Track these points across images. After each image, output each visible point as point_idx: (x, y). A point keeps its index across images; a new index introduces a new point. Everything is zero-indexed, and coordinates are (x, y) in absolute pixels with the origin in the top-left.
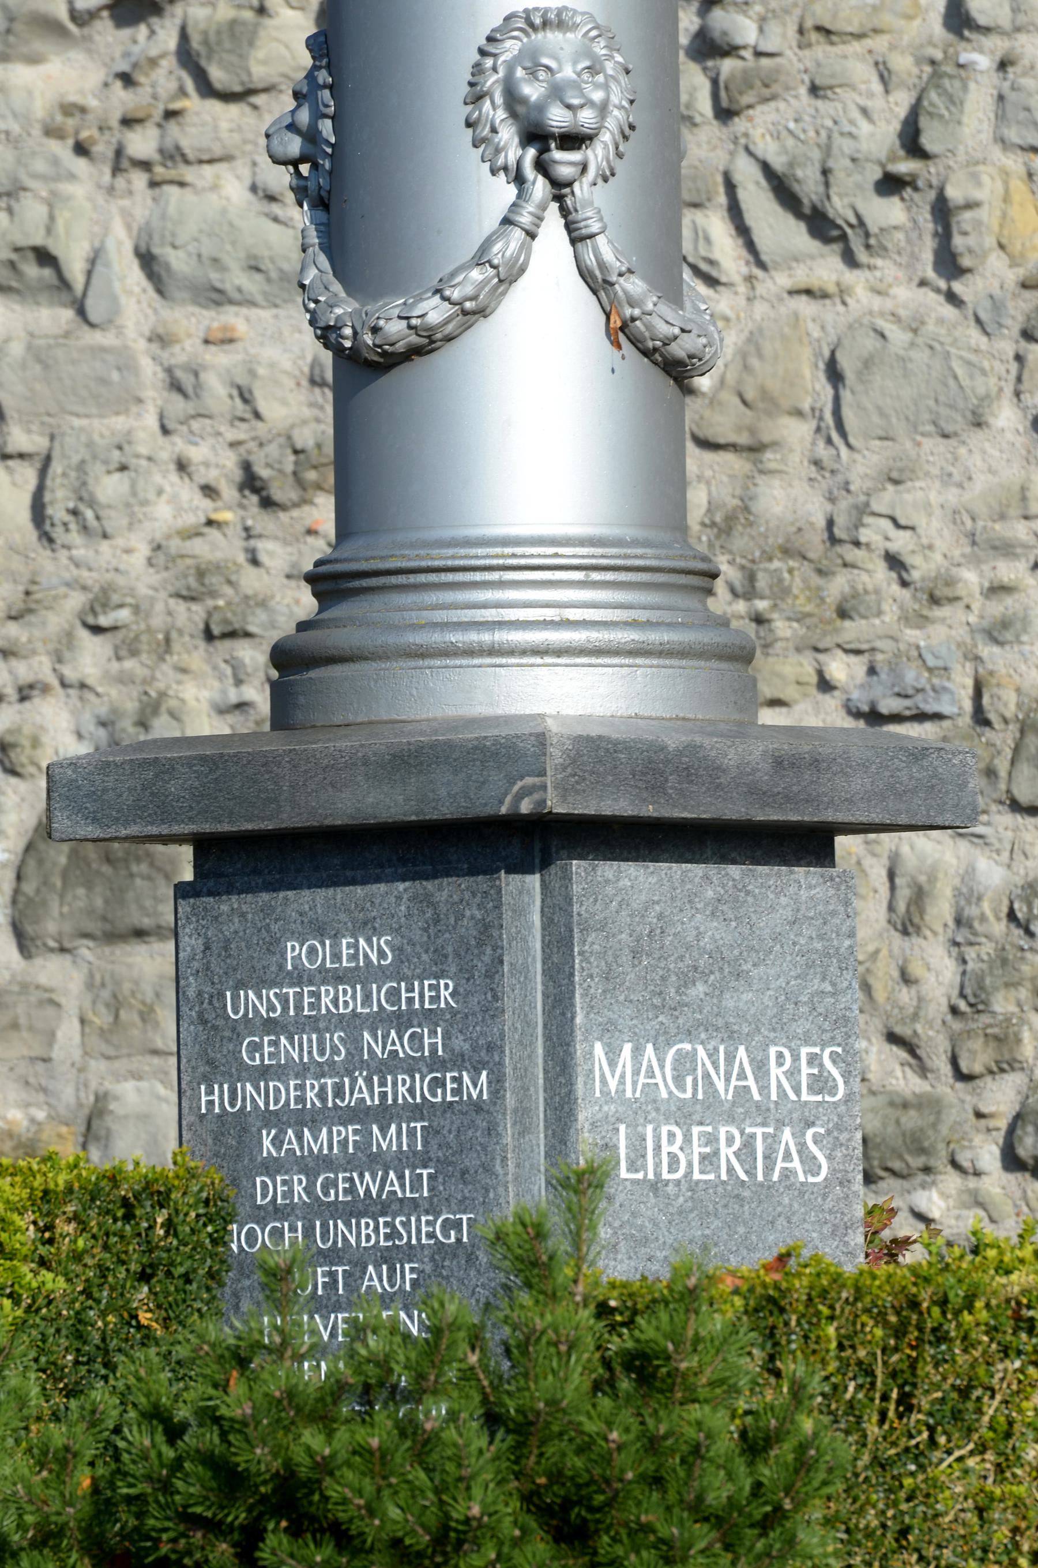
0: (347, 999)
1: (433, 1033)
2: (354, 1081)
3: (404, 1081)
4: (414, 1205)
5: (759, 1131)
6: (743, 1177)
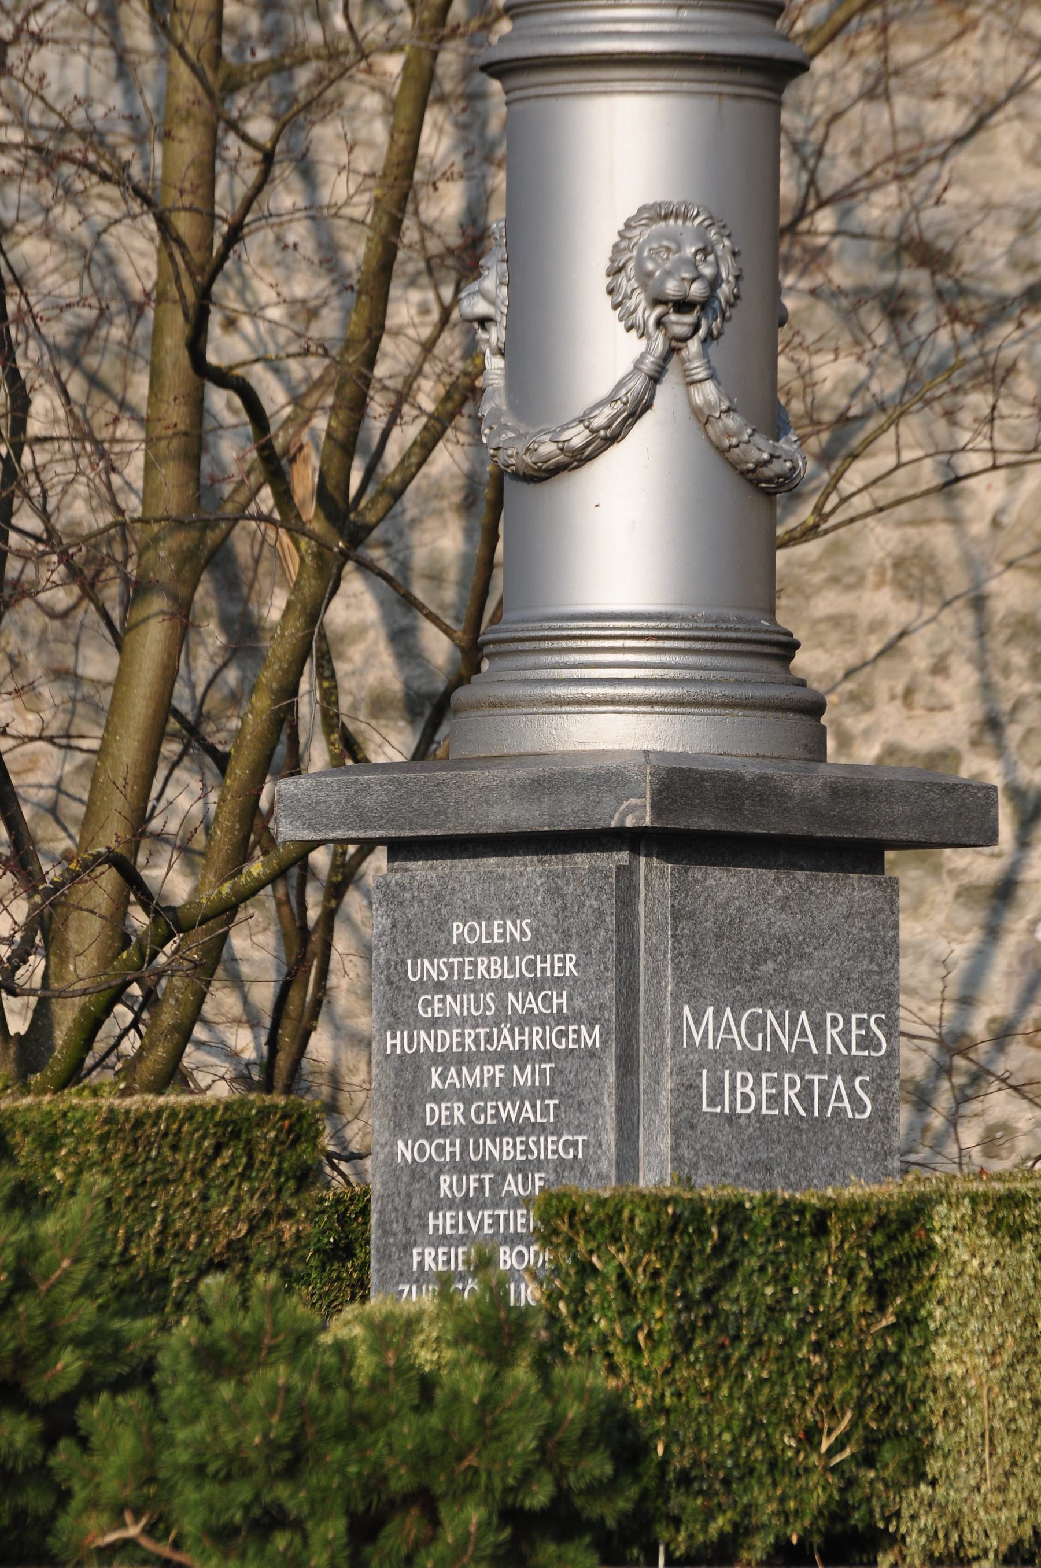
0: (496, 968)
1: (560, 995)
2: (500, 1031)
3: (835, 1021)
4: (542, 1129)
5: (816, 1078)
6: (803, 1113)
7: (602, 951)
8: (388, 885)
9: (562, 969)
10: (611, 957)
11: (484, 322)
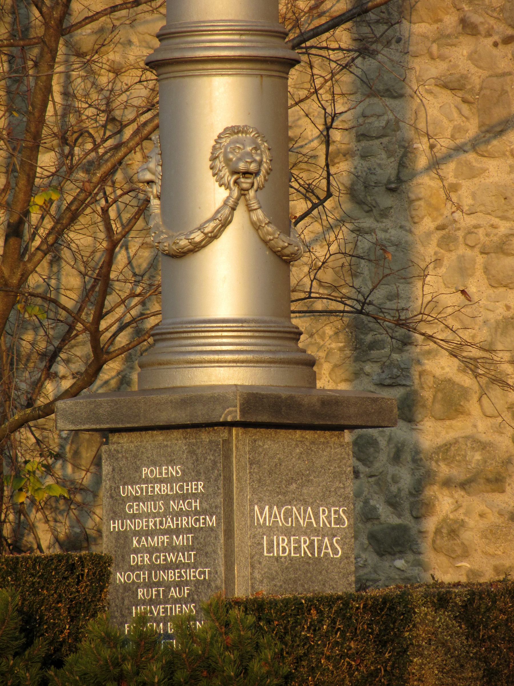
0: (164, 489)
2: (167, 520)
4: (188, 566)
5: (316, 539)
6: (310, 555)
7: (216, 480)
8: (110, 450)
9: (197, 489)
10: (221, 483)
11: (150, 182)
